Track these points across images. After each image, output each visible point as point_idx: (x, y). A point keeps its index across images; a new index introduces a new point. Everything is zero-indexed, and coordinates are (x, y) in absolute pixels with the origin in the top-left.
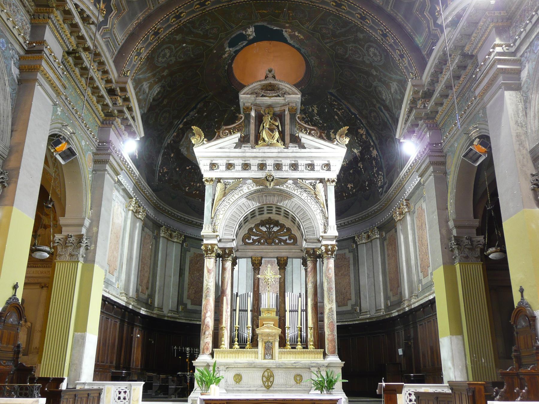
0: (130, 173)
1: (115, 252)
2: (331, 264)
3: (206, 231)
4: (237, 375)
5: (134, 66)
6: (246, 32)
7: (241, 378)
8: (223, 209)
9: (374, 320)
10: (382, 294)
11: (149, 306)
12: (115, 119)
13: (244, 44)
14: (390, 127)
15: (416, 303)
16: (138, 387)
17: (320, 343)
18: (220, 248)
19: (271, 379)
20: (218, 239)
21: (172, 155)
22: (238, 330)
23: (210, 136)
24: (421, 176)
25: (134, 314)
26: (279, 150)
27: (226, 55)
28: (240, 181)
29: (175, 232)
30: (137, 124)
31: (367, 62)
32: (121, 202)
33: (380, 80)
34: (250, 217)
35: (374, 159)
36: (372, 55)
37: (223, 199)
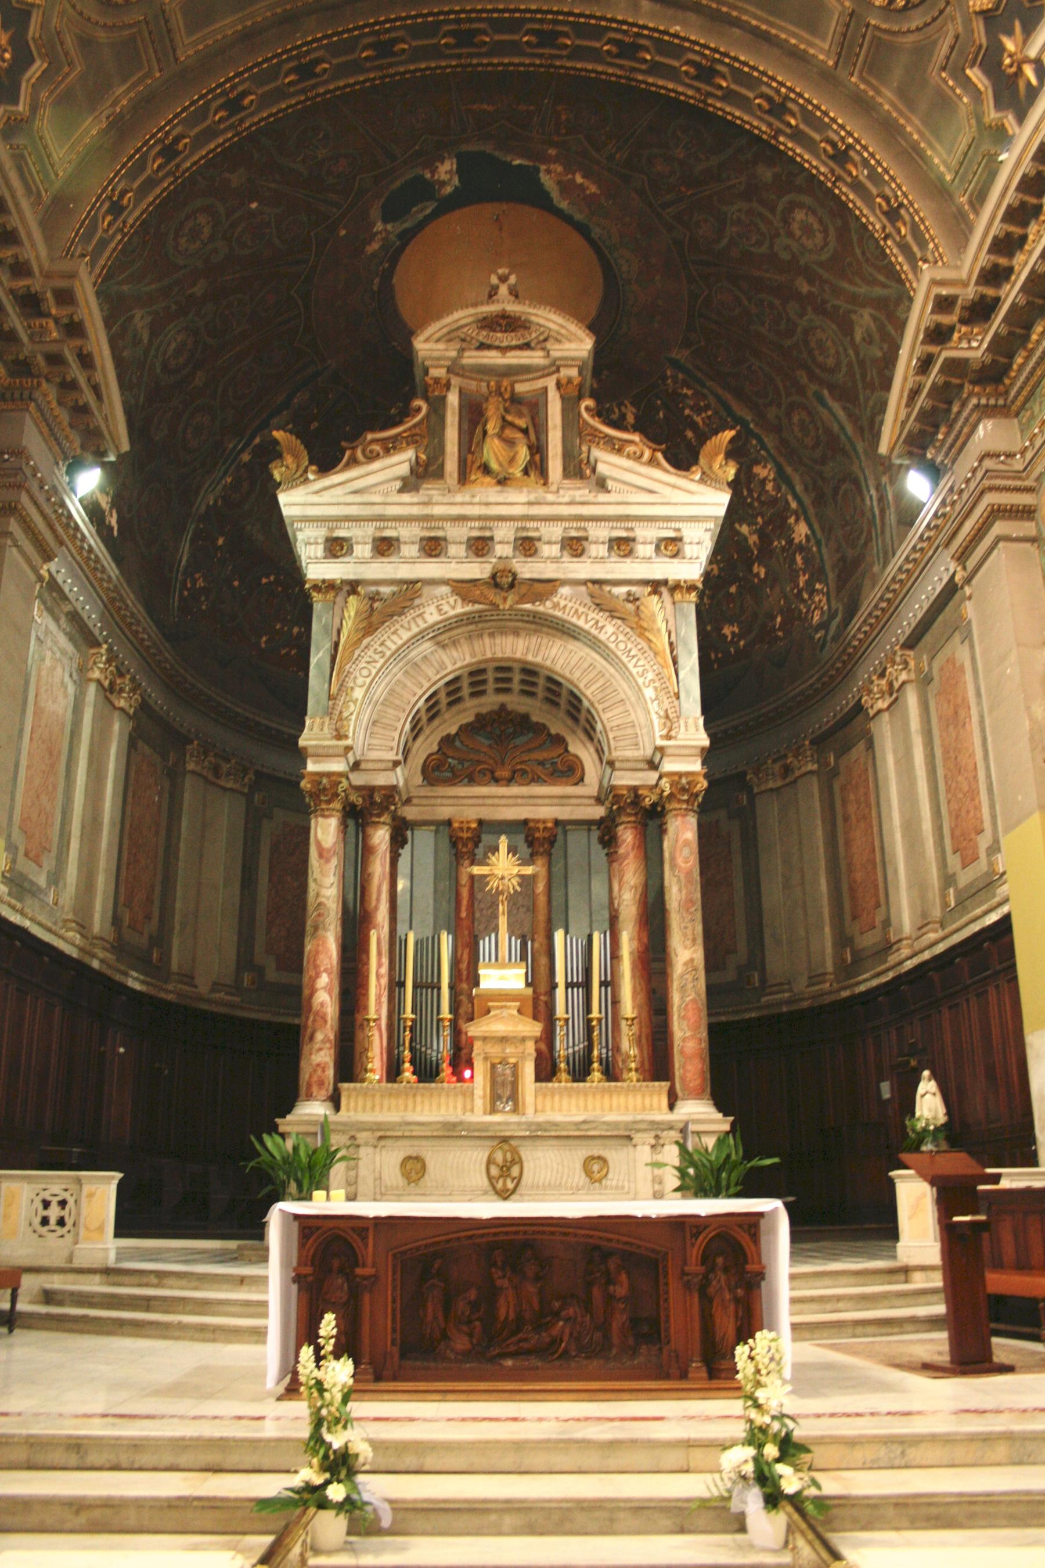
0: (87, 566)
1: (44, 798)
2: (682, 833)
3: (313, 735)
4: (409, 1158)
5: (103, 243)
6: (433, 173)
7: (424, 1167)
8: (365, 672)
9: (805, 1004)
10: (827, 930)
11: (154, 967)
12: (39, 385)
13: (428, 211)
14: (848, 447)
15: (938, 942)
16: (100, 1192)
17: (659, 1066)
18: (358, 788)
19: (515, 1171)
20: (352, 761)
21: (220, 542)
22: (411, 1028)
23: (326, 460)
24: (962, 557)
25: (108, 987)
26: (532, 497)
27: (375, 246)
28: (410, 591)
29: (228, 761)
30: (106, 409)
31: (785, 256)
32: (64, 653)
33: (821, 309)
34: (444, 700)
35: (801, 548)
36: (798, 233)
37: (365, 642)
